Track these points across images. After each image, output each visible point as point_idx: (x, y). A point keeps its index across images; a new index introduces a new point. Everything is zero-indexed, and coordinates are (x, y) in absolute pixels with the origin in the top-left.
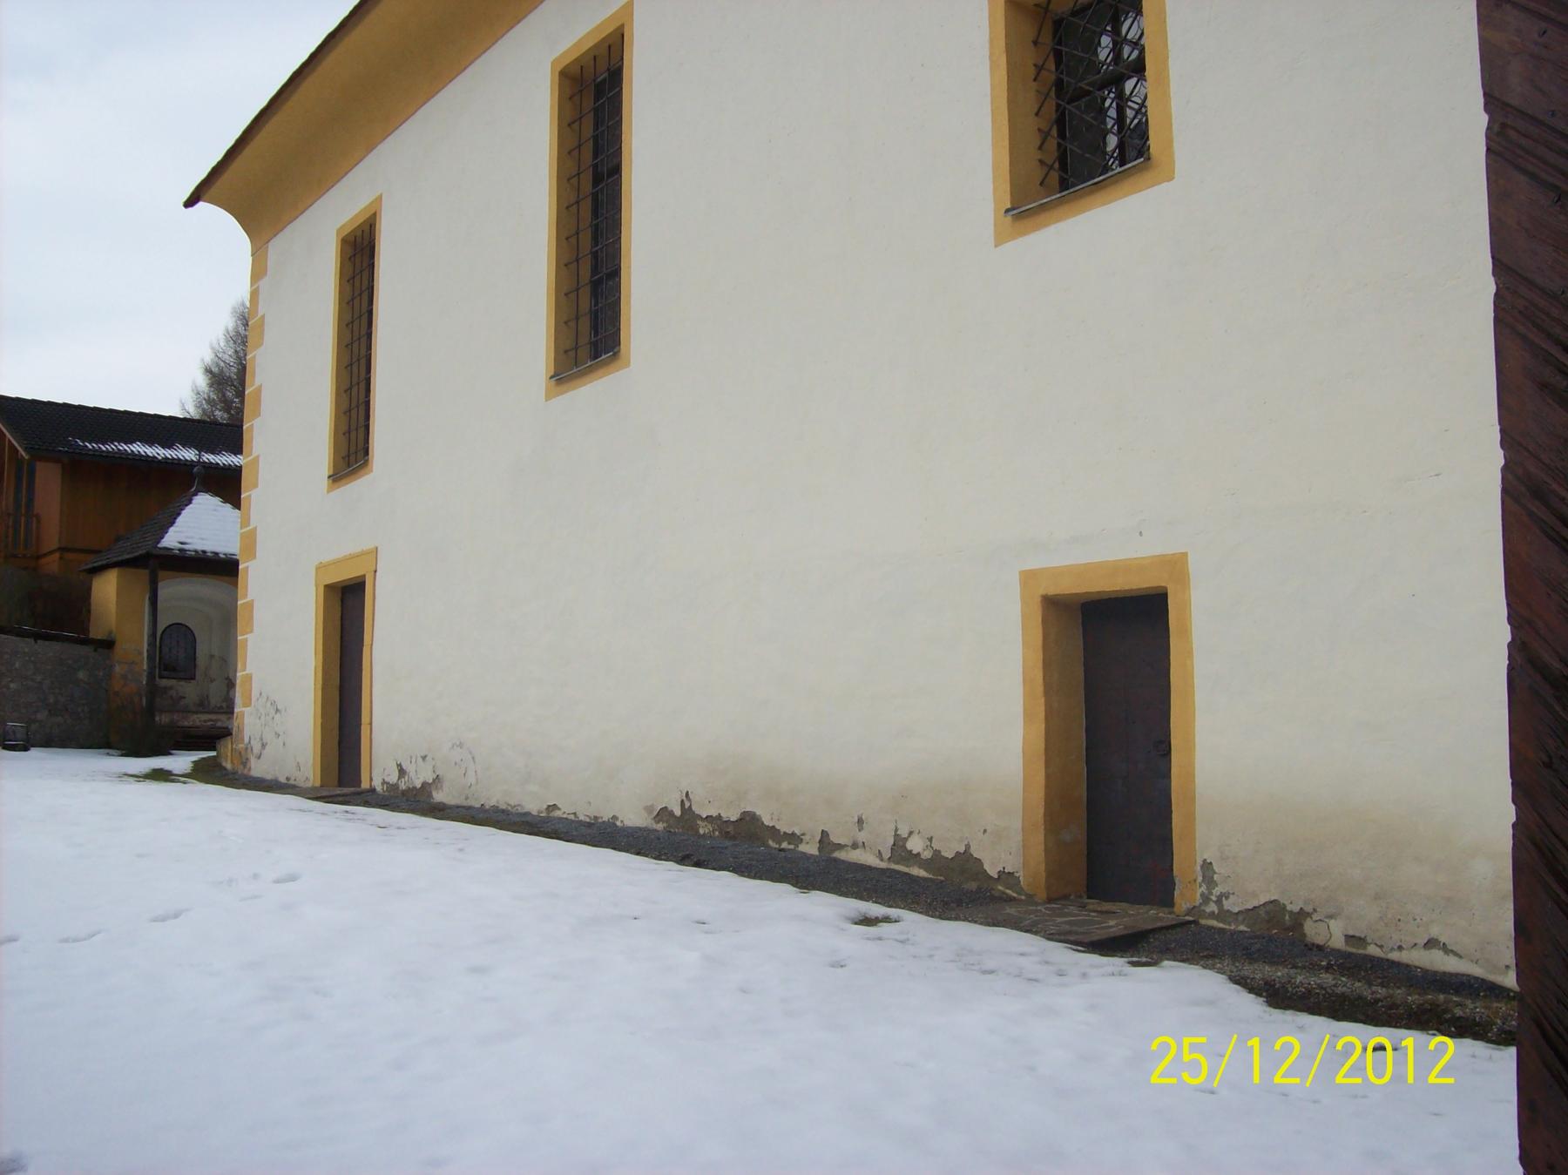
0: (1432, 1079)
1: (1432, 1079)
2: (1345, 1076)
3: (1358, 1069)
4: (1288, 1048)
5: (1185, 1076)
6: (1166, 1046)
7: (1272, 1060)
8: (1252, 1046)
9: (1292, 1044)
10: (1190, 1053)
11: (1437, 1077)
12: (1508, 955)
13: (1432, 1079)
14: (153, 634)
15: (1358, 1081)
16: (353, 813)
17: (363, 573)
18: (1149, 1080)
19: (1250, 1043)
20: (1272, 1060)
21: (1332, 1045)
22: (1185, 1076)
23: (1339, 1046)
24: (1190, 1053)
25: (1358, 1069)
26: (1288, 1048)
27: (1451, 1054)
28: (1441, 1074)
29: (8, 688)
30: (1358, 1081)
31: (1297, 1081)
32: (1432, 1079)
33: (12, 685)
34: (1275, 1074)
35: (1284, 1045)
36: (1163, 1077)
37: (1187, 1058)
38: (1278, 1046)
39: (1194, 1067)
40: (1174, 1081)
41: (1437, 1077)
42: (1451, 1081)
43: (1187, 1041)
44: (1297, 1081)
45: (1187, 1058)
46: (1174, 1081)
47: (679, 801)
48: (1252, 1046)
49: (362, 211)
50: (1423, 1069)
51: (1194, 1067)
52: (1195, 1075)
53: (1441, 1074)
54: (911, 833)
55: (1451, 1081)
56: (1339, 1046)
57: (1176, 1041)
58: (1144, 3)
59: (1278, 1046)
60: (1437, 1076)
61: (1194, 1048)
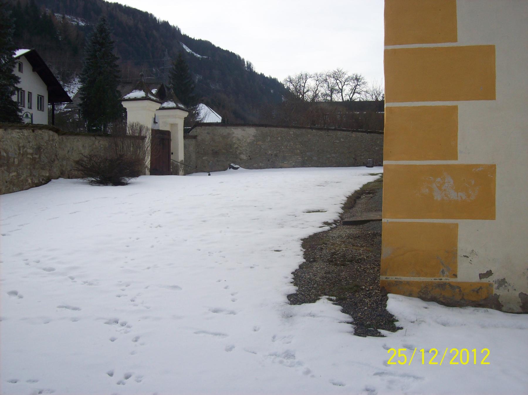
0: (482, 363)
1: (482, 363)
2: (432, 362)
3: (457, 360)
4: (486, 352)
5: (399, 362)
6: (454, 352)
7: (480, 356)
8: (422, 352)
9: (456, 351)
10: (401, 354)
13: (482, 363)
15: (457, 363)
16: (75, 309)
17: (496, 98)
18: (480, 363)
19: (473, 351)
20: (480, 356)
21: (449, 351)
22: (399, 362)
23: (451, 352)
24: (401, 354)
25: (457, 360)
26: (486, 352)
27: (489, 354)
29: (375, 149)
30: (457, 363)
31: (437, 363)
32: (482, 363)
33: (376, 148)
34: (429, 361)
37: (400, 356)
38: (482, 352)
39: (402, 359)
40: (395, 363)
42: (489, 363)
43: (400, 350)
44: (437, 363)
45: (400, 356)
46: (395, 363)
48: (422, 352)
50: (479, 359)
51: (402, 359)
52: (402, 361)
55: (489, 363)
56: (451, 352)
57: (396, 350)
58: (457, 2)
59: (482, 352)
60: (432, 362)
61: (402, 352)
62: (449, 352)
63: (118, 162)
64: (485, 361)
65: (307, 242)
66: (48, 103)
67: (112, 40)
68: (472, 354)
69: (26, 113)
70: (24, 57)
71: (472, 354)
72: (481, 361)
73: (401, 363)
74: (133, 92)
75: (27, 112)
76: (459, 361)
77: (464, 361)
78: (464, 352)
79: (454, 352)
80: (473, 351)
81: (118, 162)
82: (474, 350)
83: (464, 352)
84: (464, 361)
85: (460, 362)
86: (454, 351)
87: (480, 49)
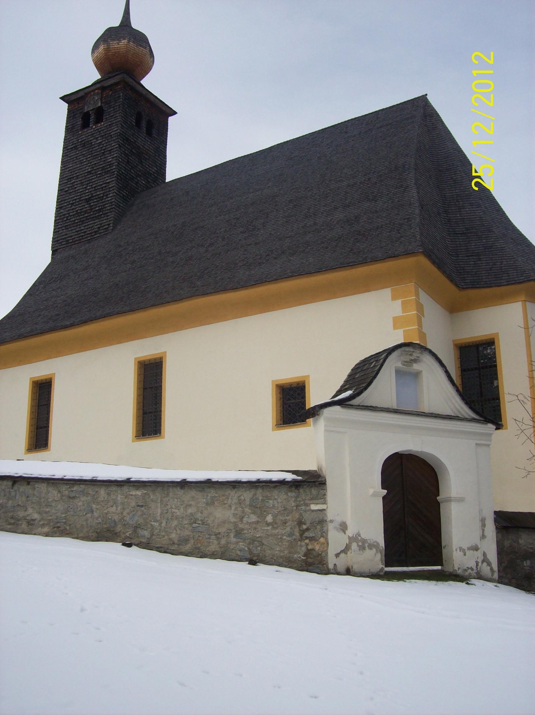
4: (477, 57)
6: (477, 99)
8: (477, 74)
9: (475, 58)
11: (490, 102)
12: (312, 406)
14: (472, 420)
15: (492, 95)
19: (475, 75)
20: (483, 65)
22: (490, 175)
23: (477, 104)
25: (487, 96)
26: (477, 57)
28: (489, 128)
30: (492, 95)
31: (492, 124)
32: (491, 62)
35: (476, 101)
36: (491, 433)
40: (492, 180)
41: (490, 102)
42: (492, 53)
44: (492, 124)
46: (492, 180)
47: (55, 475)
48: (477, 74)
49: (501, 361)
53: (489, 128)
54: (205, 518)
55: (492, 53)
56: (477, 104)
59: (477, 62)
62: (475, 64)
64: (490, 129)
65: (256, 244)
68: (480, 76)
70: (351, 574)
71: (480, 76)
72: (489, 64)
73: (492, 171)
76: (489, 93)
78: (477, 86)
79: (477, 99)
82: (475, 73)
83: (477, 86)
84: (488, 86)
85: (490, 92)
86: (475, 58)
87: (308, 376)
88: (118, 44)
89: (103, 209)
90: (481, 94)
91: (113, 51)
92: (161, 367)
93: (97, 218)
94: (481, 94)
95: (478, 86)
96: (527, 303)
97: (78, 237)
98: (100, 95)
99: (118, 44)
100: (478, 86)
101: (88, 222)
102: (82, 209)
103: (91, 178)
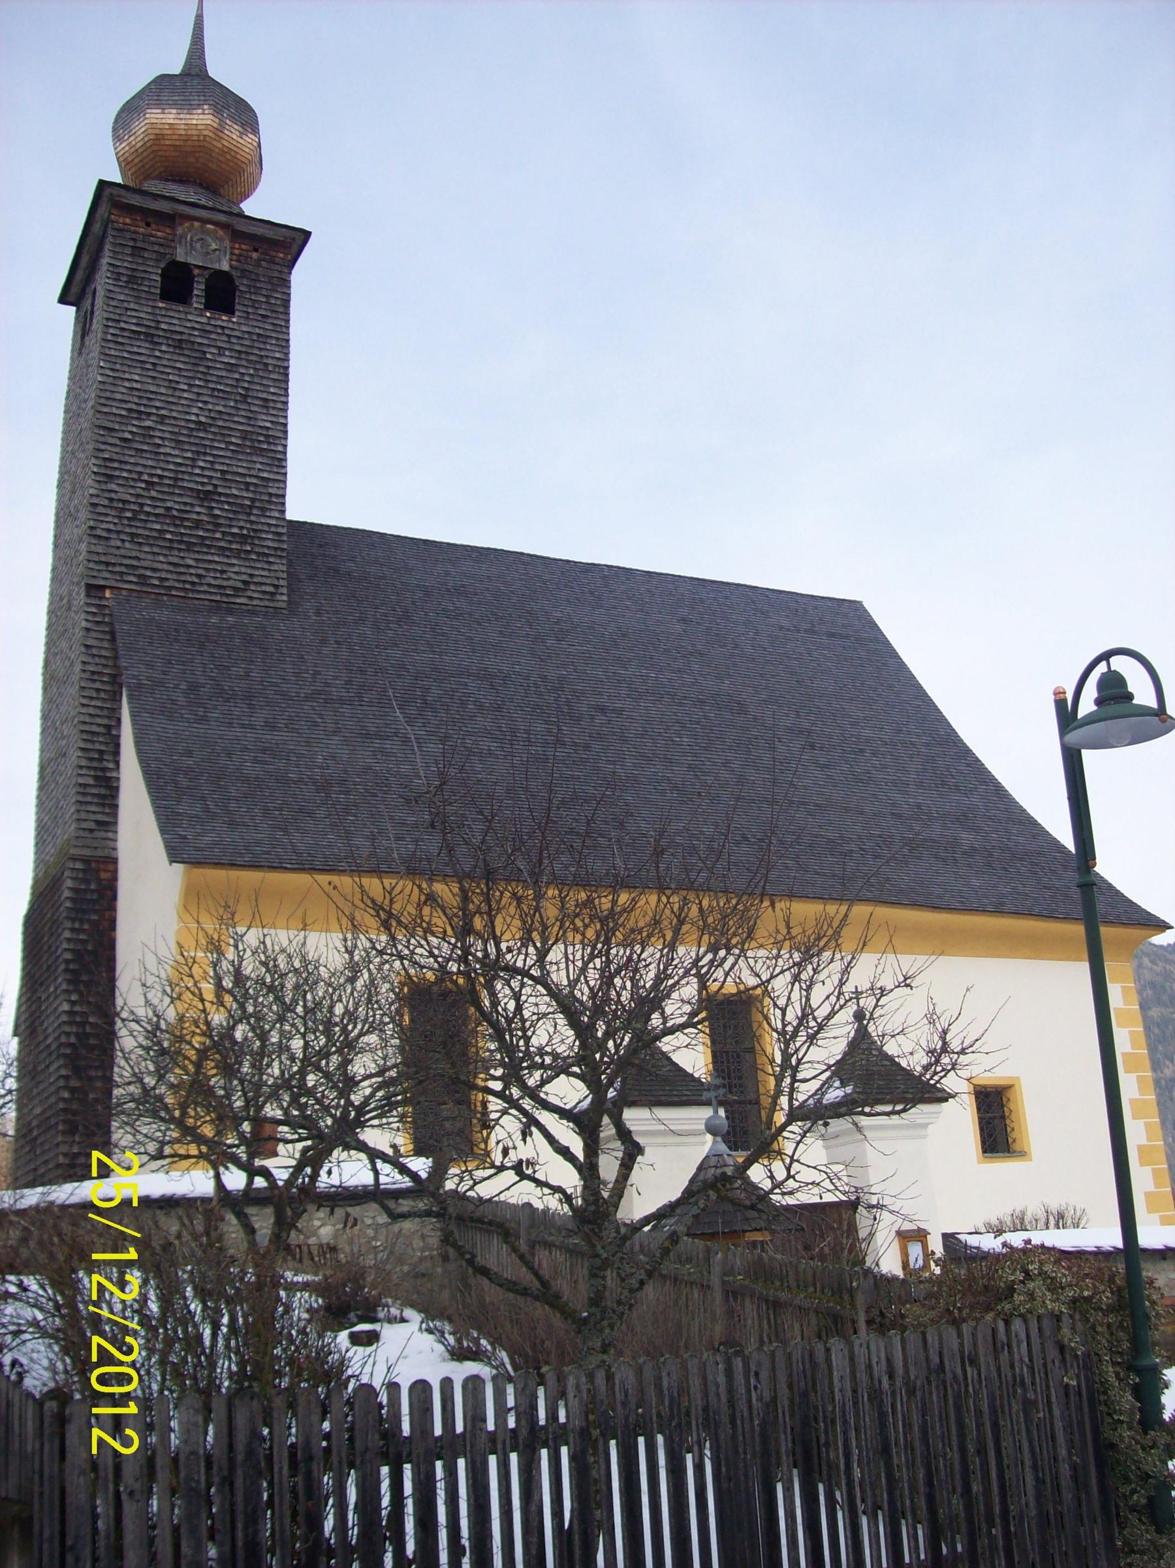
3: (106, 1358)
4: (127, 1442)
7: (117, 1425)
15: (94, 1359)
20: (117, 1425)
25: (106, 1358)
26: (127, 1442)
30: (94, 1359)
38: (128, 1432)
63: (282, 937)
66: (139, 1198)
67: (778, 905)
68: (124, 1399)
69: (1102, 668)
74: (862, 1234)
75: (1106, 656)
76: (99, 1364)
77: (102, 1380)
80: (132, 1404)
81: (282, 937)
84: (102, 1380)
88: (241, 135)
89: (253, 538)
90: (121, 1363)
91: (226, 143)
92: (983, 1143)
93: (238, 554)
94: (121, 1363)
95: (124, 1379)
96: (362, 1137)
97: (178, 581)
98: (491, 1098)
99: (241, 135)
100: (124, 1379)
101: (207, 553)
102: (186, 512)
103: (208, 443)
